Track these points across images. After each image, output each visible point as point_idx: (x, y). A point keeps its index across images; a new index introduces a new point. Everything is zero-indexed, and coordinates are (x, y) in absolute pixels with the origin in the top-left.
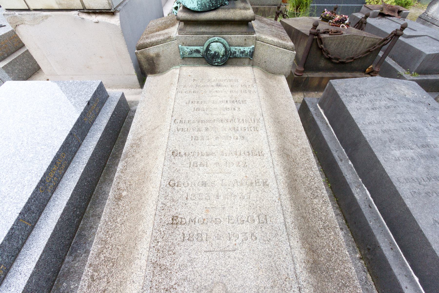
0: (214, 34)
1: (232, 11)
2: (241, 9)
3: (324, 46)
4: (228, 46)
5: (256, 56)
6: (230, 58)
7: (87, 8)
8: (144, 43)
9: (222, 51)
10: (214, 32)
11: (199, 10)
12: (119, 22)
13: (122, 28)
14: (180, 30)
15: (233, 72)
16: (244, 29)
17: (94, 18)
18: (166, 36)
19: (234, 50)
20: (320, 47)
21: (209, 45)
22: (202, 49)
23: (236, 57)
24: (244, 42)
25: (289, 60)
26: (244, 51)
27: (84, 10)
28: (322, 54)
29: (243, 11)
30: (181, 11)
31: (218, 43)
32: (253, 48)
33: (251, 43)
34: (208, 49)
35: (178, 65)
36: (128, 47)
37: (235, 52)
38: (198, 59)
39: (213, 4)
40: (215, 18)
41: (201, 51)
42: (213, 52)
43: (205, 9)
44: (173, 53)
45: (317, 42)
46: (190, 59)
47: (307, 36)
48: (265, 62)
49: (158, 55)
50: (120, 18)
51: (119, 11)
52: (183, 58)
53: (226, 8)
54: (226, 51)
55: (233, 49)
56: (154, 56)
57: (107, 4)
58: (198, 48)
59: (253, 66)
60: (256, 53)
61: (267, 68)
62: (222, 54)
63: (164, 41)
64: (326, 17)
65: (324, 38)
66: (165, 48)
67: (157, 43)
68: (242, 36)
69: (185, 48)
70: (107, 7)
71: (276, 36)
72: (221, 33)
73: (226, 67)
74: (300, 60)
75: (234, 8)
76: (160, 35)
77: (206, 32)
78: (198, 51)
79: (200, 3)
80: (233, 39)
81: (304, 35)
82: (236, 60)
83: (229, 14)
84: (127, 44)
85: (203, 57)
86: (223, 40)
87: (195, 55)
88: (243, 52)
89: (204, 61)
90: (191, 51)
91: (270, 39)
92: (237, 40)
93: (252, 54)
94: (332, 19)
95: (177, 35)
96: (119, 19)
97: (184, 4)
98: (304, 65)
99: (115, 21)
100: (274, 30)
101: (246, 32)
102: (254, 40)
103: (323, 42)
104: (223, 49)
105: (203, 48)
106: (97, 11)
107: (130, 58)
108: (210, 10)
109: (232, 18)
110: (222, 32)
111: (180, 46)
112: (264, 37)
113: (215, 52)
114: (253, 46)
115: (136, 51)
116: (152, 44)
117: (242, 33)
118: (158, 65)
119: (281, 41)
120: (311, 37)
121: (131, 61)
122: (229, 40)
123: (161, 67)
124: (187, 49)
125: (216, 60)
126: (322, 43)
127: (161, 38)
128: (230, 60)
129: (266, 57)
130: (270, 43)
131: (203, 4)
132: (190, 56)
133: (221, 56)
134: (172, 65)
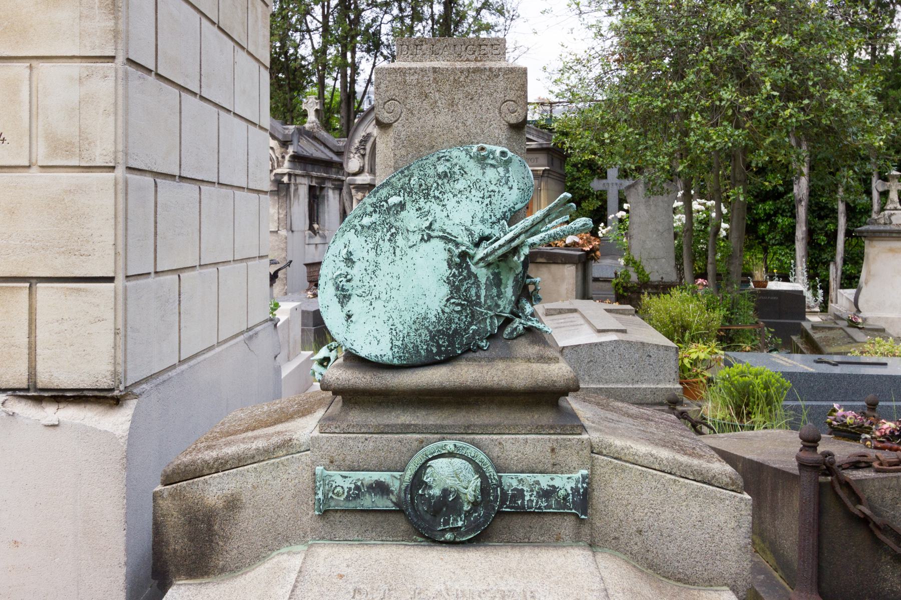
0: (442, 431)
1: (501, 365)
2: (529, 360)
3: (871, 508)
4: (490, 471)
5: (601, 507)
6: (500, 513)
7: (40, 385)
8: (194, 462)
9: (470, 487)
10: (442, 427)
11: (396, 362)
12: (127, 425)
13: (129, 445)
14: (325, 424)
15: (513, 565)
16: (546, 417)
17: (51, 413)
18: (275, 440)
19: (515, 483)
20: (857, 512)
21: (424, 467)
22: (394, 480)
23: (523, 512)
24: (548, 459)
25: (733, 524)
26: (553, 490)
27: (28, 390)
28: (878, 542)
29: (536, 367)
30: (339, 366)
31: (457, 461)
32: (584, 478)
33: (574, 460)
34: (418, 481)
35: (303, 540)
36: (128, 506)
37: (520, 493)
38: (380, 518)
39: (439, 346)
40: (446, 384)
41: (395, 486)
42: (436, 492)
43: (415, 360)
44: (288, 495)
45: (836, 494)
46: (350, 517)
47: (794, 476)
48: (640, 532)
49: (233, 504)
50: (134, 416)
51: (137, 396)
52: (325, 513)
53: (480, 359)
54: (485, 488)
55: (511, 481)
56: (220, 504)
57: (108, 374)
58: (376, 476)
59: (592, 545)
60: (599, 496)
61: (650, 556)
62: (471, 498)
63: (267, 454)
64: (845, 424)
65: (859, 481)
66: (266, 476)
67: (240, 461)
68: (540, 437)
69: (337, 477)
70: (105, 383)
71: (664, 443)
72: (467, 429)
73: (488, 549)
74: (796, 566)
75: (509, 357)
76: (256, 438)
77: (415, 425)
78: (381, 488)
79: (399, 343)
80: (508, 446)
81: (780, 474)
82: (528, 521)
83: (493, 372)
84: (128, 497)
85: (399, 510)
86: (472, 451)
87: (368, 502)
88: (548, 494)
89: (402, 525)
90: (357, 488)
91: (642, 449)
92: (525, 455)
93: (584, 499)
94: (868, 430)
95: (316, 433)
96: (130, 418)
97: (348, 346)
98: (819, 586)
99: (116, 422)
100: (654, 430)
101: (552, 427)
102: (587, 452)
103: (864, 497)
104: (475, 482)
105: (401, 479)
106: (68, 394)
107: (122, 547)
108: (431, 363)
109: (504, 383)
110: (468, 427)
111: (319, 469)
112: (618, 443)
113: (446, 492)
114: (585, 472)
115: (160, 488)
116: (222, 466)
117: (538, 430)
118: (226, 539)
119: (684, 459)
120: (807, 477)
121: (123, 559)
122: (496, 452)
123: (232, 550)
124: (343, 481)
125: (446, 522)
126: (859, 501)
127: (261, 444)
128: (500, 524)
129: (638, 514)
130: (645, 463)
131: (411, 346)
132: (351, 505)
133: (466, 507)
134: (280, 538)
